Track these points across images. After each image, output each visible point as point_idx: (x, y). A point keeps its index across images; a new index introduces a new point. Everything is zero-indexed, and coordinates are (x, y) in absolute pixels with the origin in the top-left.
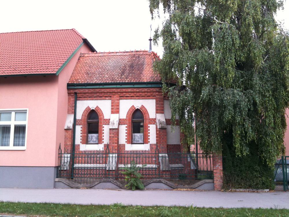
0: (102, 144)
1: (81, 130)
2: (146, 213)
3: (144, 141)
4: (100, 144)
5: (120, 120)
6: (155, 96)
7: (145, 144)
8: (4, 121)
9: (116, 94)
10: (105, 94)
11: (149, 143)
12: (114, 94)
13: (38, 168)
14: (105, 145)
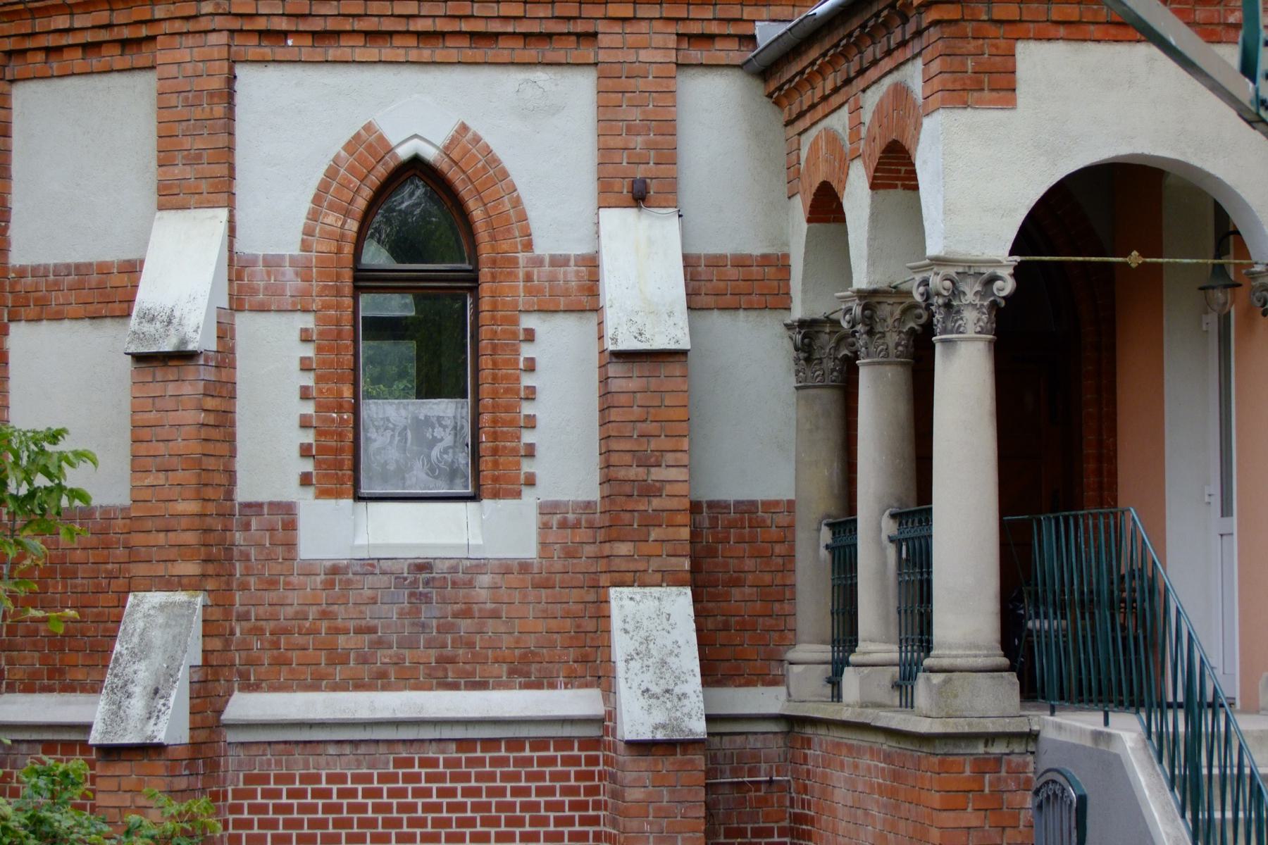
0: (517, 495)
1: (303, 360)
3: (477, 485)
4: (496, 495)
7: (487, 503)
8: (856, 488)
11: (526, 492)
14: (547, 509)
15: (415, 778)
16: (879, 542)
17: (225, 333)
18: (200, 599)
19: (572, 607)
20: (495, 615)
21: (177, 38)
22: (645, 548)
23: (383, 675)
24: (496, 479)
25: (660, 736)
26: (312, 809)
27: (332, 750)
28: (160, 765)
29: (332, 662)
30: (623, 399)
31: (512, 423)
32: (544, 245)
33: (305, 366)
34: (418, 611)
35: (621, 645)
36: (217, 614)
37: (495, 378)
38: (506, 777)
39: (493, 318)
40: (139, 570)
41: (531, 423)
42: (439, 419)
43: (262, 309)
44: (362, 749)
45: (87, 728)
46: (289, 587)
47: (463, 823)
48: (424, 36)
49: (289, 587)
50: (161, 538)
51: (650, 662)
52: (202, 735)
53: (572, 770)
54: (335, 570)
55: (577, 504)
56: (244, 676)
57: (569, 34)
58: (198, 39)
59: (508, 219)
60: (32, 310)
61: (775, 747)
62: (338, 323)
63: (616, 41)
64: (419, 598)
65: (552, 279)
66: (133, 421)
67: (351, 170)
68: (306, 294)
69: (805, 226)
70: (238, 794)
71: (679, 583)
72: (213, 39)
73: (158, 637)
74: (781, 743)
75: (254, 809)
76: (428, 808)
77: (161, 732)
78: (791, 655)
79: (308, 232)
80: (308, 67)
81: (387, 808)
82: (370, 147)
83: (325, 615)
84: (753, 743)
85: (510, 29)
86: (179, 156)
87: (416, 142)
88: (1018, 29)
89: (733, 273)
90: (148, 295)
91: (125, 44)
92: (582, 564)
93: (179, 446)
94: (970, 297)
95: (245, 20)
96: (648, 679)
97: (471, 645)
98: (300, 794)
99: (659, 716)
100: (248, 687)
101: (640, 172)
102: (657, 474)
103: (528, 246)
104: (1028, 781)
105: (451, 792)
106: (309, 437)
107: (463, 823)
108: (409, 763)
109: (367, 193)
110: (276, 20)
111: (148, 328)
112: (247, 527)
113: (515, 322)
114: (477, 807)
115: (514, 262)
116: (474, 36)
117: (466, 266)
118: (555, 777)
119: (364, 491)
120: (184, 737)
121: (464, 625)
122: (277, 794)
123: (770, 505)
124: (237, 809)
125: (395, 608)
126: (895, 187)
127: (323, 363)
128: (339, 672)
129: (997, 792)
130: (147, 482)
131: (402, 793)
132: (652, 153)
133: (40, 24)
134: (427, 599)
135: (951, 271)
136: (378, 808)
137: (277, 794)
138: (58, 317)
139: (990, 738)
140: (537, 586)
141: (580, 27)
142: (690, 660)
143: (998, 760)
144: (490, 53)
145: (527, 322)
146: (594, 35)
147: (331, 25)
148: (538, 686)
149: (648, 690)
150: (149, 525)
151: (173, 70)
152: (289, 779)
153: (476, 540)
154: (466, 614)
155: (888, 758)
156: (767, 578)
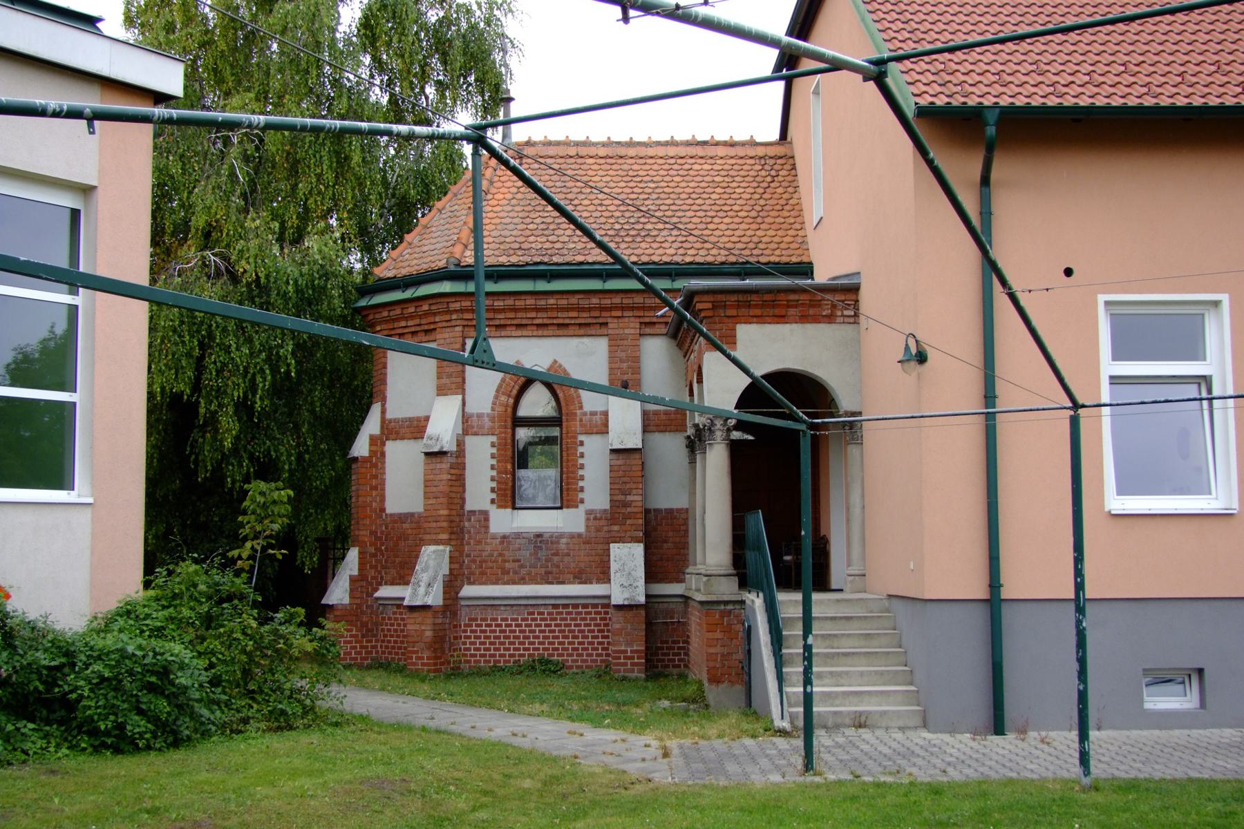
0: (577, 507)
2: (96, 740)
4: (568, 507)
9: (626, 314)
10: (520, 315)
12: (619, 313)
13: (1055, 604)
14: (589, 512)
15: (535, 619)
17: (460, 444)
18: (448, 549)
20: (568, 555)
22: (624, 528)
23: (523, 579)
24: (568, 501)
25: (626, 603)
26: (495, 631)
27: (502, 608)
28: (430, 614)
29: (503, 574)
33: (493, 456)
35: (614, 566)
36: (457, 554)
38: (572, 619)
40: (427, 537)
41: (582, 478)
43: (476, 434)
44: (515, 608)
45: (403, 599)
46: (486, 544)
47: (554, 637)
48: (539, 326)
49: (486, 544)
50: (434, 525)
52: (449, 602)
53: (598, 616)
54: (504, 537)
55: (600, 510)
56: (469, 579)
58: (451, 329)
60: (394, 436)
61: (681, 608)
62: (505, 439)
63: (615, 326)
65: (591, 420)
68: (493, 428)
70: (466, 625)
71: (639, 542)
72: (457, 329)
73: (432, 563)
75: (472, 631)
76: (541, 631)
77: (430, 601)
78: (688, 571)
79: (494, 403)
81: (524, 631)
83: (500, 555)
84: (672, 606)
88: (737, 319)
89: (663, 417)
90: (431, 430)
91: (426, 332)
92: (602, 534)
93: (441, 488)
96: (623, 580)
97: (558, 566)
98: (490, 625)
99: (626, 595)
100: (470, 583)
101: (625, 377)
102: (629, 498)
103: (581, 408)
105: (550, 625)
106: (494, 484)
107: (554, 637)
108: (533, 613)
109: (517, 387)
111: (429, 442)
112: (469, 520)
113: (576, 438)
114: (560, 631)
115: (576, 414)
116: (559, 325)
118: (591, 619)
119: (517, 506)
120: (440, 602)
121: (556, 559)
122: (481, 625)
123: (679, 510)
124: (465, 631)
128: (506, 578)
129: (730, 625)
131: (530, 625)
133: (396, 325)
134: (541, 548)
136: (521, 631)
137: (481, 625)
138: (403, 438)
139: (726, 603)
141: (601, 321)
142: (640, 572)
143: (730, 611)
144: (565, 332)
145: (581, 438)
146: (606, 324)
147: (502, 322)
148: (585, 583)
150: (430, 519)
152: (485, 619)
153: (560, 525)
154: (556, 554)
156: (678, 539)
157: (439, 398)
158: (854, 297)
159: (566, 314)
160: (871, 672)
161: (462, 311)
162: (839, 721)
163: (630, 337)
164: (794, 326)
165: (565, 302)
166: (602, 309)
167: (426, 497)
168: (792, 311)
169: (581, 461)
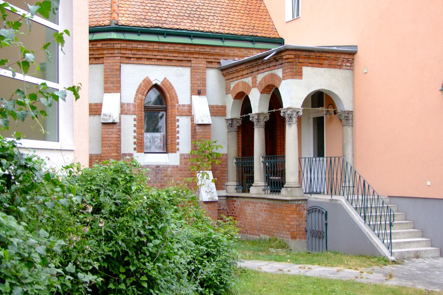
0: (176, 152)
1: (134, 124)
4: (172, 152)
5: (122, 105)
6: (299, 62)
7: (170, 154)
10: (149, 53)
11: (177, 152)
14: (181, 155)
16: (260, 162)
17: (120, 119)
19: (186, 175)
21: (109, 58)
24: (172, 149)
25: (210, 200)
30: (199, 133)
31: (175, 138)
32: (181, 102)
34: (157, 176)
37: (171, 129)
39: (171, 117)
42: (157, 137)
43: (126, 114)
51: (206, 186)
57: (186, 60)
58: (114, 58)
59: (174, 97)
63: (195, 62)
64: (157, 173)
65: (182, 109)
66: (102, 136)
67: (144, 86)
68: (135, 111)
69: (232, 100)
72: (117, 58)
74: (225, 201)
79: (135, 98)
80: (135, 65)
82: (147, 82)
85: (175, 59)
86: (109, 82)
87: (156, 81)
88: (303, 64)
89: (216, 109)
90: (105, 110)
93: (112, 142)
94: (294, 115)
95: (124, 55)
96: (206, 189)
99: (209, 196)
101: (199, 88)
103: (178, 102)
104: (305, 208)
110: (129, 55)
111: (105, 117)
113: (175, 118)
115: (175, 106)
117: (164, 106)
125: (152, 175)
126: (265, 93)
127: (138, 125)
130: (105, 149)
132: (202, 85)
134: (158, 173)
135: (291, 110)
139: (299, 200)
140: (179, 171)
141: (188, 59)
143: (300, 205)
145: (178, 118)
146: (191, 61)
147: (141, 56)
149: (206, 191)
151: (108, 64)
153: (168, 161)
154: (166, 176)
155: (267, 204)
157: (106, 94)
158: (352, 57)
159: (172, 55)
160: (407, 232)
161: (120, 49)
162: (409, 255)
163: (202, 68)
164: (326, 69)
165: (173, 48)
166: (190, 53)
167: (103, 146)
168: (326, 62)
169: (177, 129)
